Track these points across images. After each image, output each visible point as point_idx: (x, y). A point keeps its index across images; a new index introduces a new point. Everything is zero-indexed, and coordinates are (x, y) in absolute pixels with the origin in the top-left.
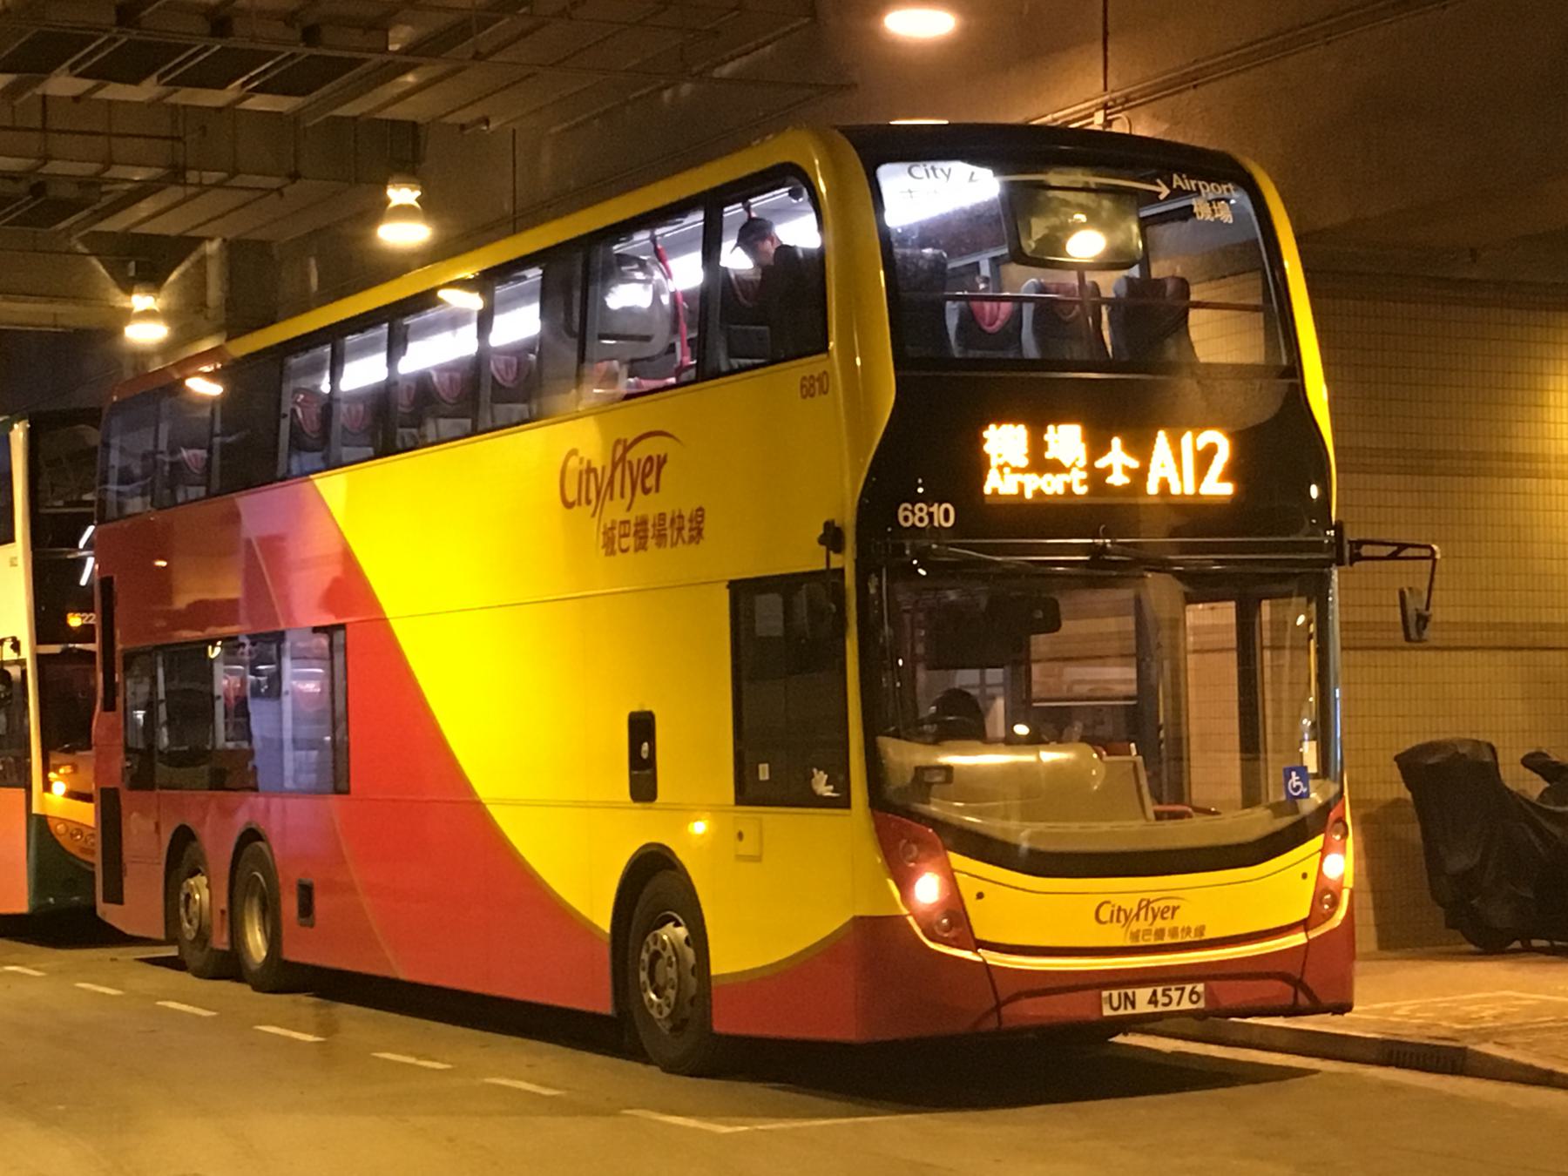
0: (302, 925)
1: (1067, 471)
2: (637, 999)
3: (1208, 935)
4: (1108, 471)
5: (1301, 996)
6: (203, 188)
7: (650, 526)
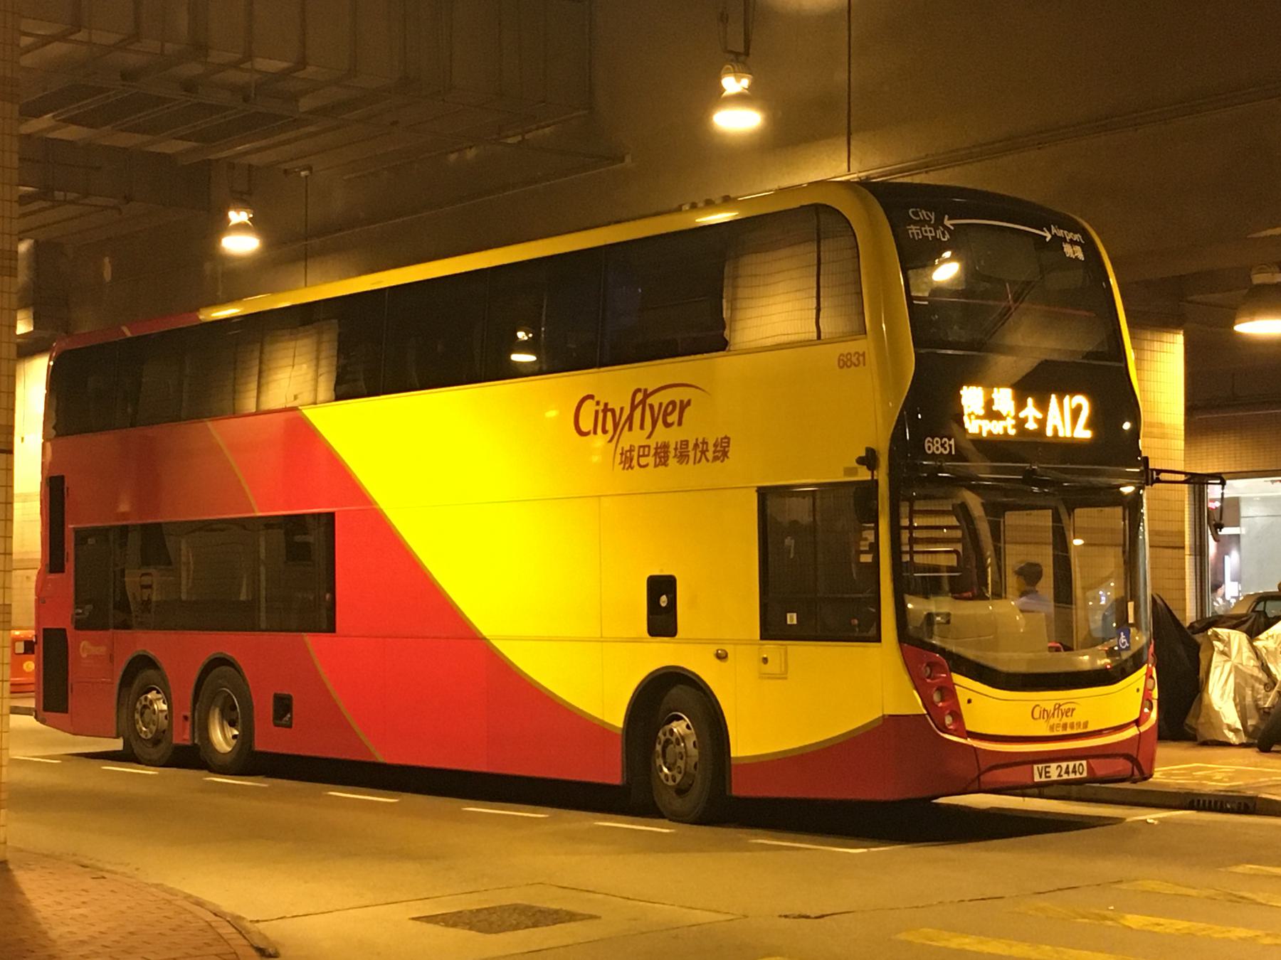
0: (276, 725)
3: (1091, 728)
4: (1025, 420)
5: (1136, 772)
6: (65, 202)
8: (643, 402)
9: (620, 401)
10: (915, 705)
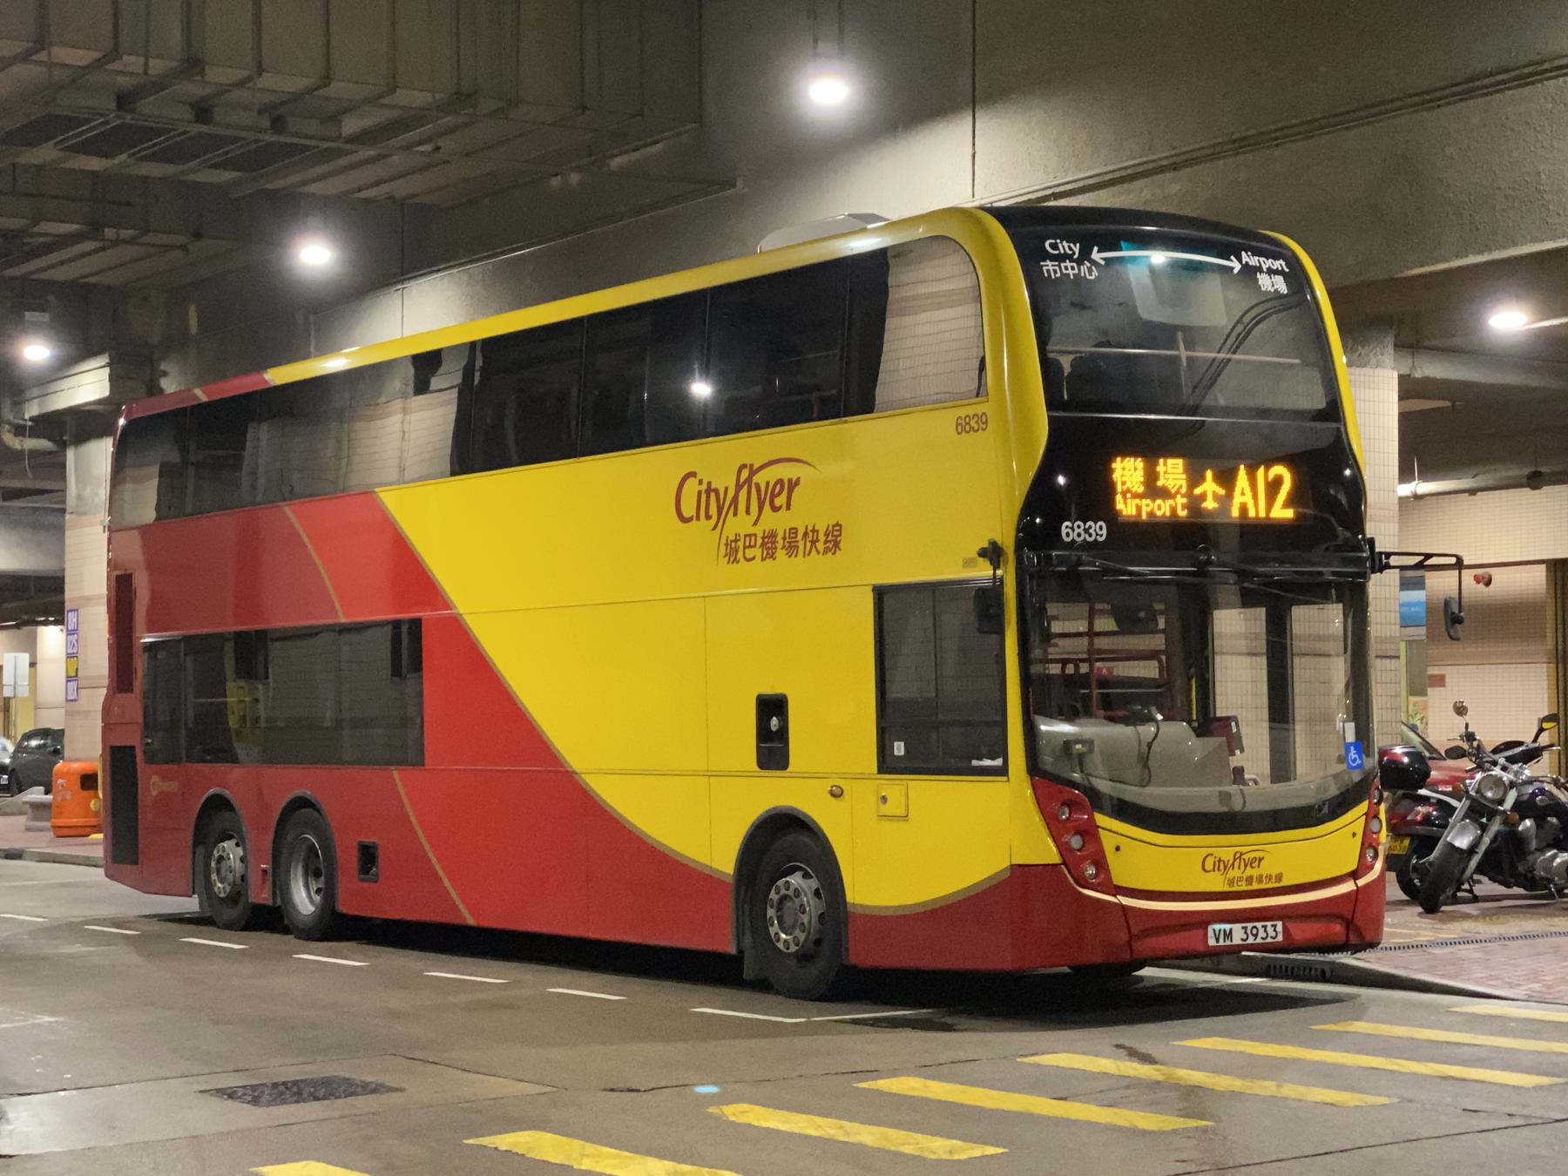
0: (363, 880)
1: (1173, 496)
2: (773, 941)
3: (1286, 882)
4: (1203, 497)
6: (116, 243)
7: (779, 539)
8: (749, 480)
9: (725, 481)
10: (1048, 853)
